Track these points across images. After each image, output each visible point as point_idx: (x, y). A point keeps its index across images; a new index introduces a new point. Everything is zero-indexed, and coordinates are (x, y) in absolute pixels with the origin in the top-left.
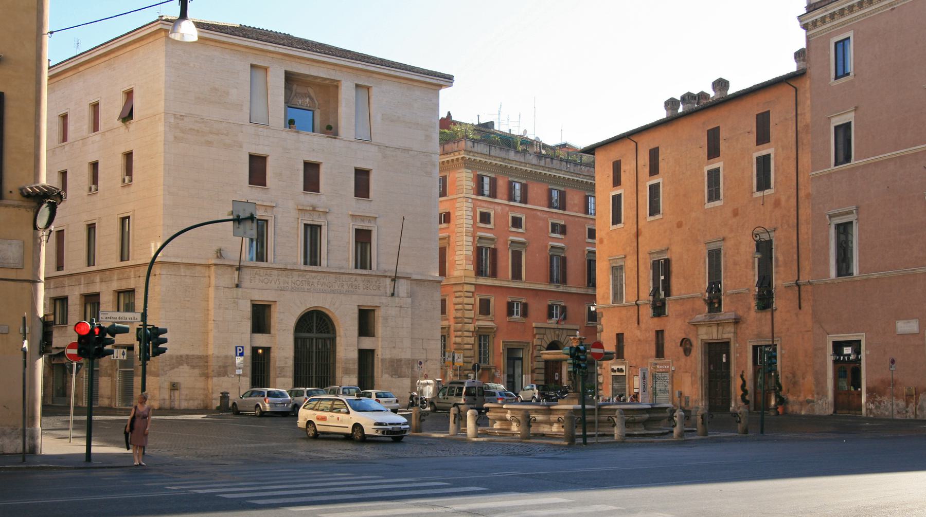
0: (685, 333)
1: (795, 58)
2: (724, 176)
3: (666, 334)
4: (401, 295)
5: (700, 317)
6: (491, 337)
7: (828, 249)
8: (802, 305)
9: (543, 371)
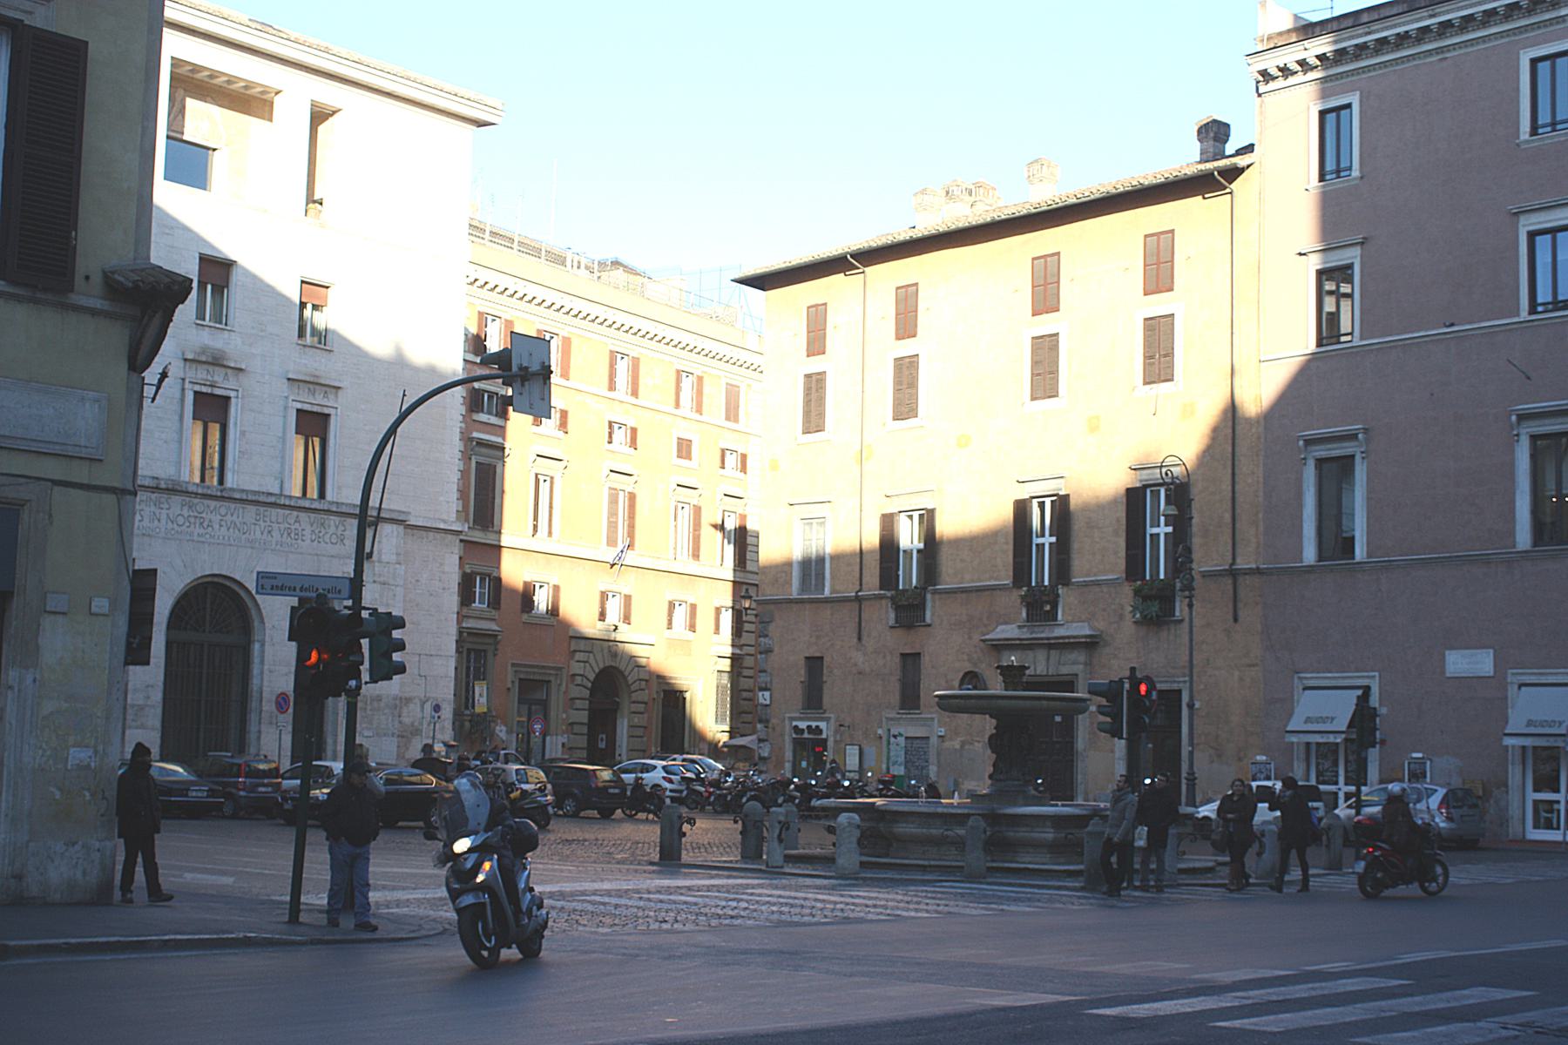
1: (1199, 131)
3: (926, 660)
4: (385, 558)
5: (1008, 631)
6: (490, 655)
8: (1241, 613)
9: (585, 730)
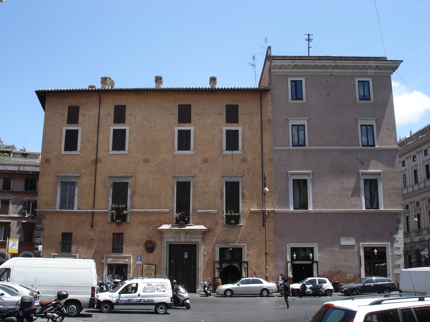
0: (148, 236)
2: (195, 137)
7: (288, 193)
